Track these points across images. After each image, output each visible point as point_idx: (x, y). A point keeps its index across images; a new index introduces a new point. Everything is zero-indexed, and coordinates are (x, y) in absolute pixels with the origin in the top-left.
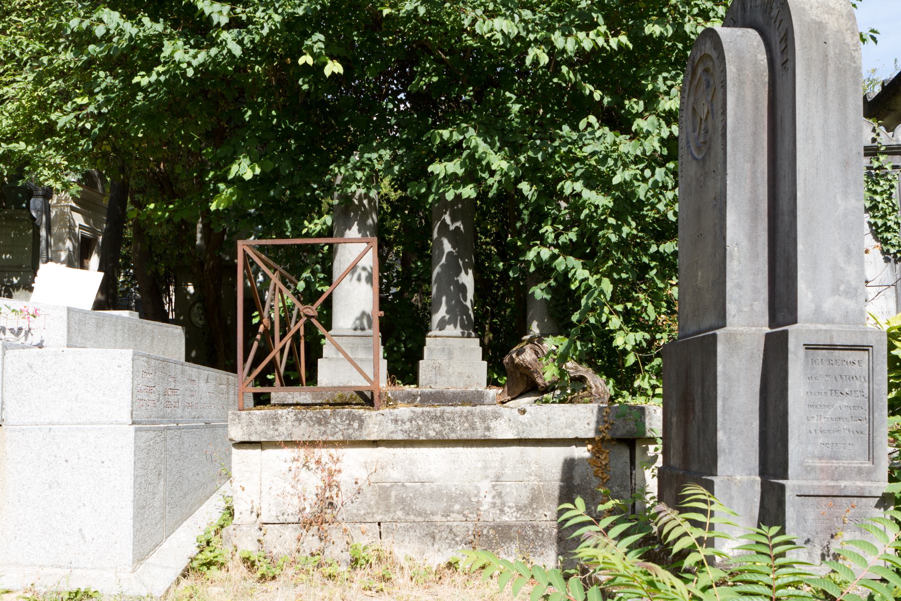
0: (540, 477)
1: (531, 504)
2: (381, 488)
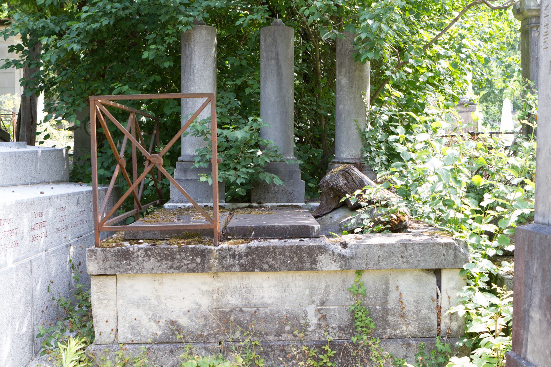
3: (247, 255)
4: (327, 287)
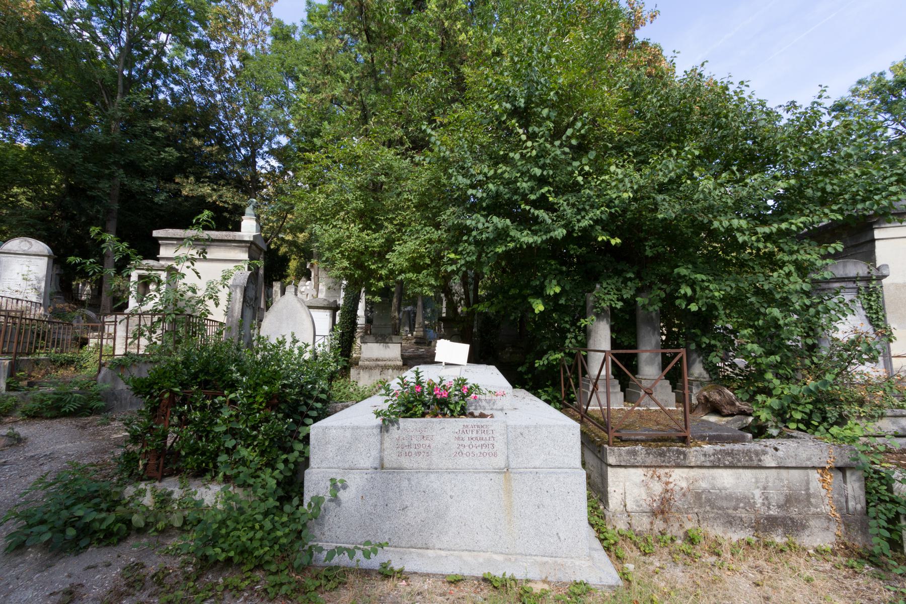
0: (789, 488)
1: (786, 504)
2: (697, 493)
3: (714, 455)
4: (767, 477)
